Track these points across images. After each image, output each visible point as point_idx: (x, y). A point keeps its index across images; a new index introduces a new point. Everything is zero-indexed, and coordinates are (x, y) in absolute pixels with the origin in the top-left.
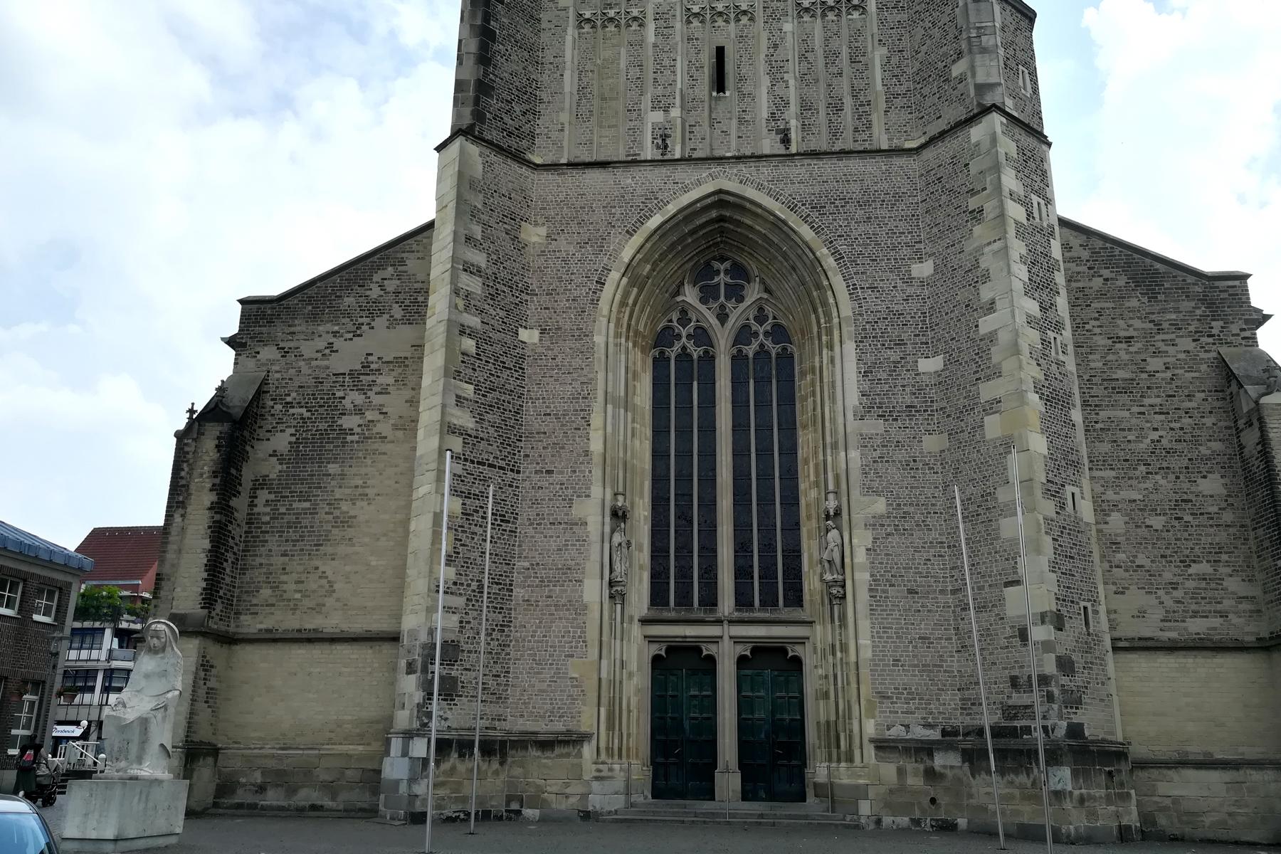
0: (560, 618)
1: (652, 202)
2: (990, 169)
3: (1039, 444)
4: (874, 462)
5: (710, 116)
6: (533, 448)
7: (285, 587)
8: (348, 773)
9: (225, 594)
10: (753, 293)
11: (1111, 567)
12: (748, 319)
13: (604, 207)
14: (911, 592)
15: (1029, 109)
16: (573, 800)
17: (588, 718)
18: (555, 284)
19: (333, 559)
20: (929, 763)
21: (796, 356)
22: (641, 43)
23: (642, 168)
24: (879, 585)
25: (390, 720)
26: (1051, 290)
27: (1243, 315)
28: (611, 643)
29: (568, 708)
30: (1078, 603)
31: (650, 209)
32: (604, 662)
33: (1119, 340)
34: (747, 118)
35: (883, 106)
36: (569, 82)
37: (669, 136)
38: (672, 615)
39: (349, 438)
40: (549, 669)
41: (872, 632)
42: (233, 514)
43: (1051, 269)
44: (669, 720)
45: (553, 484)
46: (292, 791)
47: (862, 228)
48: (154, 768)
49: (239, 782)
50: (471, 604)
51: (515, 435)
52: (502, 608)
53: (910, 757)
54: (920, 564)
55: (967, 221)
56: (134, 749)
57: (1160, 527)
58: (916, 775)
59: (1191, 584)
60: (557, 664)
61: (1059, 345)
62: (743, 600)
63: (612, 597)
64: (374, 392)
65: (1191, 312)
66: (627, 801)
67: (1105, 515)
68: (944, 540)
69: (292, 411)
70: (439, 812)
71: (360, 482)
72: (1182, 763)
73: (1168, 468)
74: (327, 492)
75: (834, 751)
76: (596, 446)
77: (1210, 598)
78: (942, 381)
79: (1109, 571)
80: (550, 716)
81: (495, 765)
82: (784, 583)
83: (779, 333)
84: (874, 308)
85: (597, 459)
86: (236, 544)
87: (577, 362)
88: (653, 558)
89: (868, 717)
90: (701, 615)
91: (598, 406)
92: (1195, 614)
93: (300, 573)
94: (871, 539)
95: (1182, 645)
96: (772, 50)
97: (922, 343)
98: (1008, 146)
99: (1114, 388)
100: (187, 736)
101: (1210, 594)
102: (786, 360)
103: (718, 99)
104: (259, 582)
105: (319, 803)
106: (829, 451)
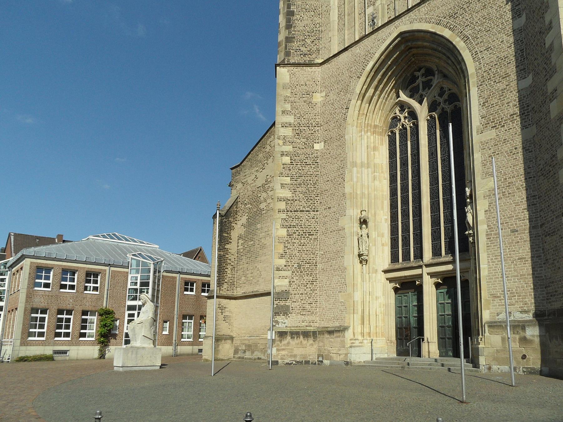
14: (514, 231)
16: (342, 356)
20: (522, 334)
24: (493, 231)
28: (361, 283)
29: (340, 316)
39: (263, 212)
41: (488, 260)
42: (228, 251)
44: (403, 318)
45: (331, 213)
46: (253, 352)
50: (294, 274)
52: (312, 274)
60: (335, 296)
62: (436, 252)
68: (536, 194)
69: (246, 206)
70: (282, 361)
80: (333, 320)
94: (488, 204)
105: (260, 357)
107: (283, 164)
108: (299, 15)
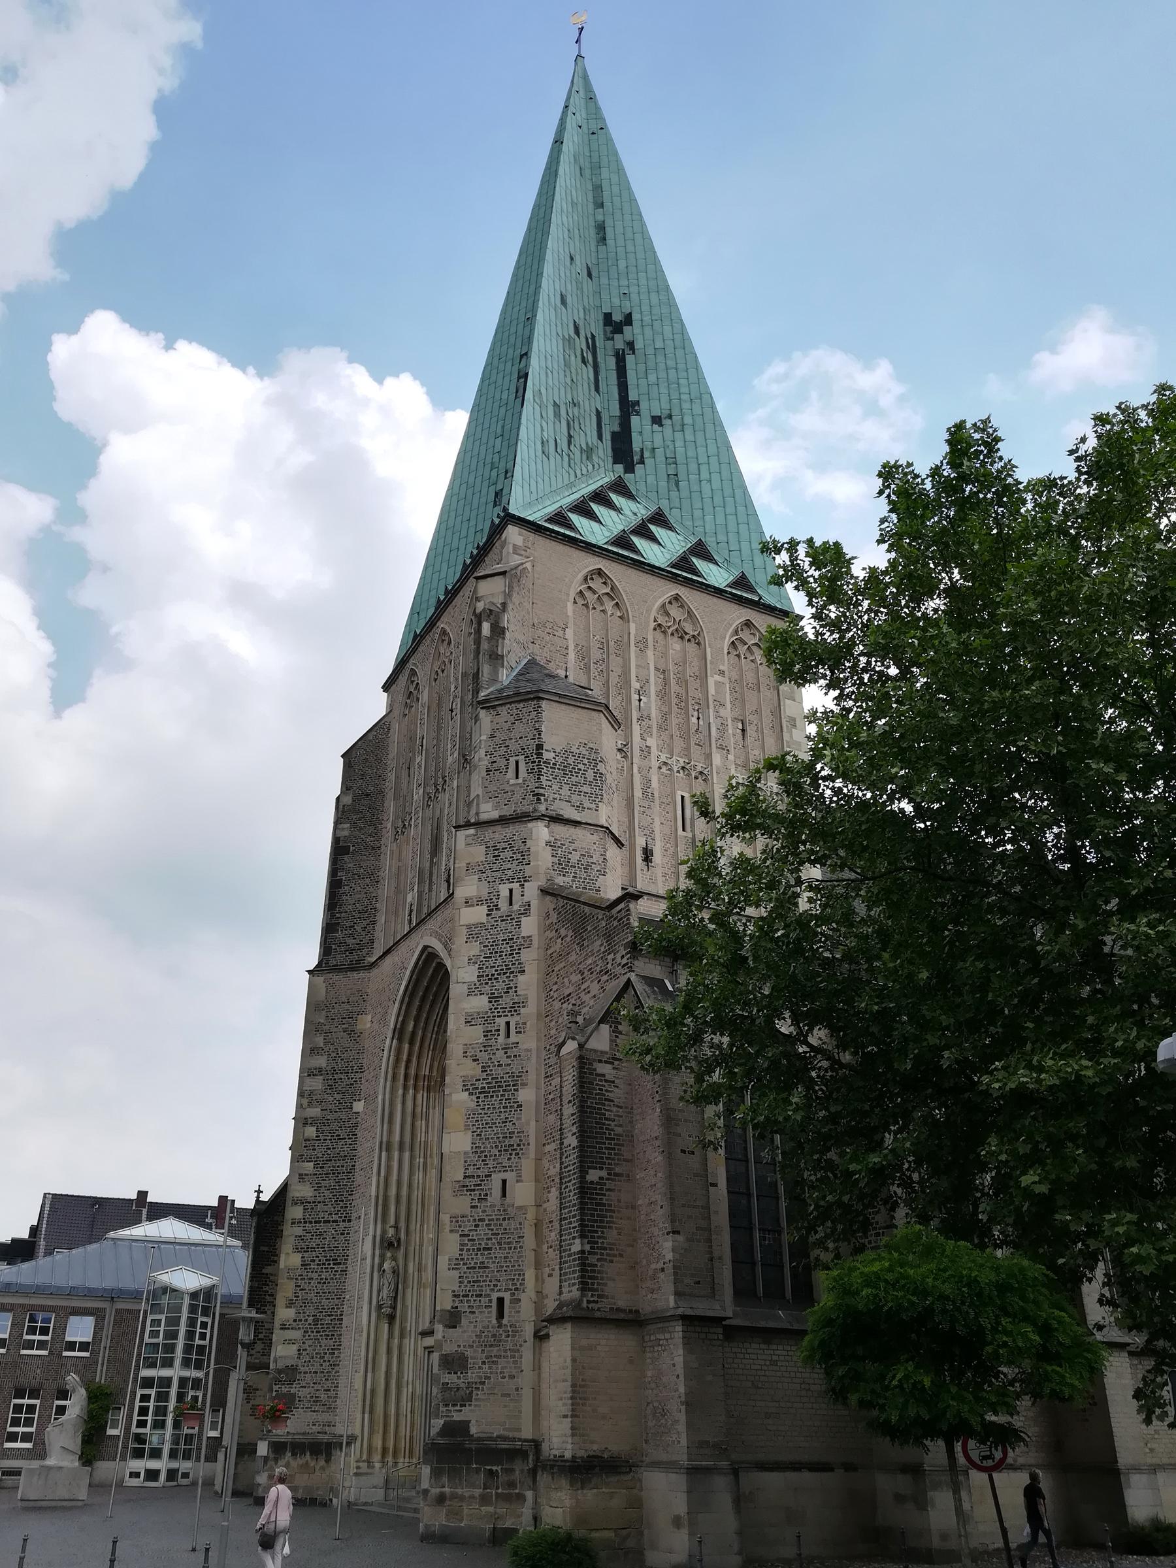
30: (489, 1296)
81: (322, 1463)
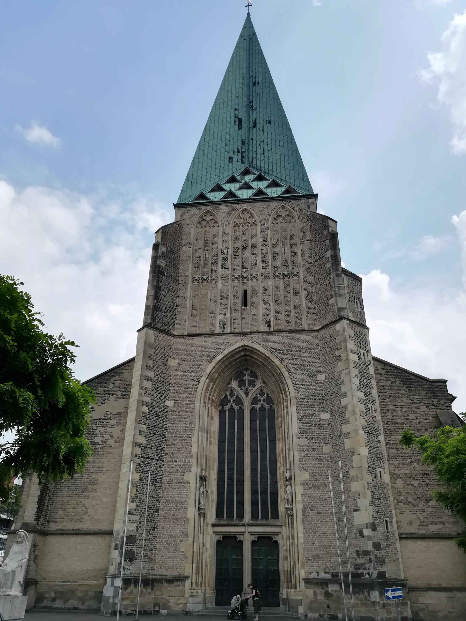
0: (178, 525)
1: (219, 349)
2: (343, 341)
3: (364, 451)
4: (304, 457)
5: (241, 316)
6: (169, 450)
7: (68, 510)
8: (89, 593)
9: (44, 514)
10: (259, 384)
11: (398, 502)
12: (257, 394)
13: (200, 352)
14: (319, 513)
15: (359, 316)
17: (188, 569)
18: (181, 382)
19: (88, 498)
20: (326, 589)
21: (275, 409)
22: (216, 288)
23: (215, 337)
25: (107, 569)
26: (370, 387)
27: (445, 397)
30: (383, 519)
31: (218, 352)
32: (195, 544)
33: (397, 406)
34: (255, 317)
35: (306, 313)
36: (189, 303)
37: (226, 324)
38: (225, 522)
39: (98, 446)
40: (173, 547)
43: (369, 379)
45: (176, 466)
46: (66, 601)
47: (298, 360)
48: (16, 591)
49: (45, 596)
50: (141, 519)
51: (162, 445)
53: (319, 586)
54: (322, 501)
55: (336, 360)
56: (9, 583)
57: (417, 485)
58: (321, 594)
59: (430, 510)
60: (176, 545)
61: (373, 410)
62: (254, 515)
63: (199, 515)
64: (108, 427)
65: (425, 395)
66: (203, 607)
67: (395, 480)
70: (125, 611)
71: (100, 465)
72: (429, 589)
73: (419, 460)
74: (88, 469)
75: (290, 584)
76: (194, 449)
77: (438, 516)
78: (330, 423)
79: (398, 504)
80: (172, 568)
81: (149, 590)
82: (271, 508)
83: (269, 400)
84: (303, 393)
85: (194, 455)
86: (50, 492)
87: (188, 414)
88: (218, 497)
89: (302, 569)
90: (237, 522)
91: (195, 433)
92: (432, 523)
93: (75, 504)
95: (427, 536)
96: (264, 292)
97: (322, 407)
98: (350, 332)
99: (396, 427)
100: (26, 576)
101: (437, 514)
102: (272, 411)
103: (244, 309)
104: (58, 508)
105: (77, 606)
106: (287, 451)
107: (143, 413)
108: (164, 291)
